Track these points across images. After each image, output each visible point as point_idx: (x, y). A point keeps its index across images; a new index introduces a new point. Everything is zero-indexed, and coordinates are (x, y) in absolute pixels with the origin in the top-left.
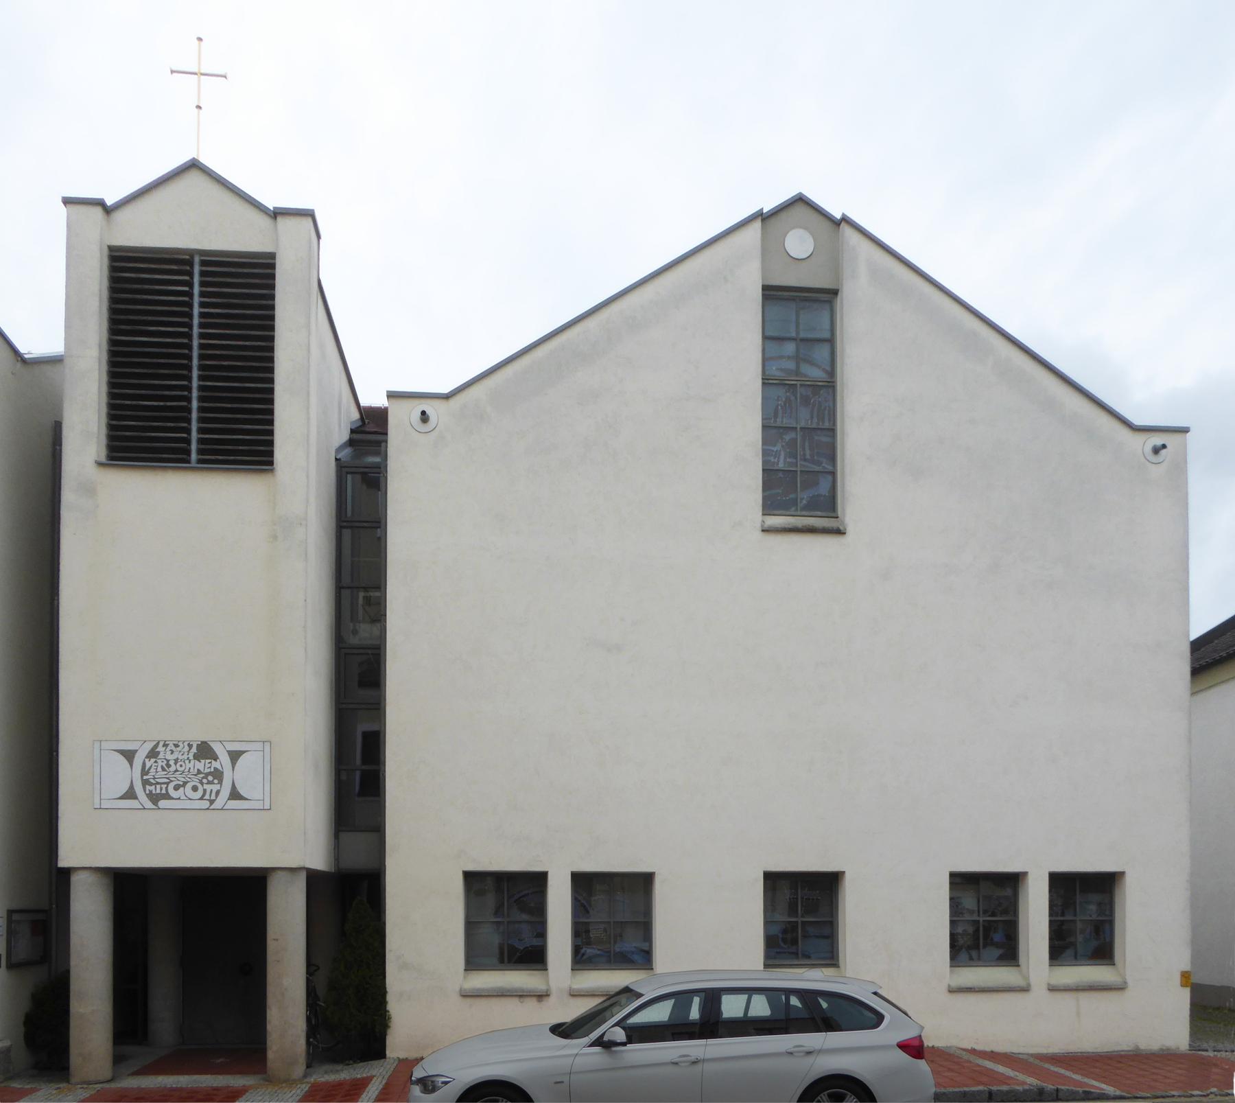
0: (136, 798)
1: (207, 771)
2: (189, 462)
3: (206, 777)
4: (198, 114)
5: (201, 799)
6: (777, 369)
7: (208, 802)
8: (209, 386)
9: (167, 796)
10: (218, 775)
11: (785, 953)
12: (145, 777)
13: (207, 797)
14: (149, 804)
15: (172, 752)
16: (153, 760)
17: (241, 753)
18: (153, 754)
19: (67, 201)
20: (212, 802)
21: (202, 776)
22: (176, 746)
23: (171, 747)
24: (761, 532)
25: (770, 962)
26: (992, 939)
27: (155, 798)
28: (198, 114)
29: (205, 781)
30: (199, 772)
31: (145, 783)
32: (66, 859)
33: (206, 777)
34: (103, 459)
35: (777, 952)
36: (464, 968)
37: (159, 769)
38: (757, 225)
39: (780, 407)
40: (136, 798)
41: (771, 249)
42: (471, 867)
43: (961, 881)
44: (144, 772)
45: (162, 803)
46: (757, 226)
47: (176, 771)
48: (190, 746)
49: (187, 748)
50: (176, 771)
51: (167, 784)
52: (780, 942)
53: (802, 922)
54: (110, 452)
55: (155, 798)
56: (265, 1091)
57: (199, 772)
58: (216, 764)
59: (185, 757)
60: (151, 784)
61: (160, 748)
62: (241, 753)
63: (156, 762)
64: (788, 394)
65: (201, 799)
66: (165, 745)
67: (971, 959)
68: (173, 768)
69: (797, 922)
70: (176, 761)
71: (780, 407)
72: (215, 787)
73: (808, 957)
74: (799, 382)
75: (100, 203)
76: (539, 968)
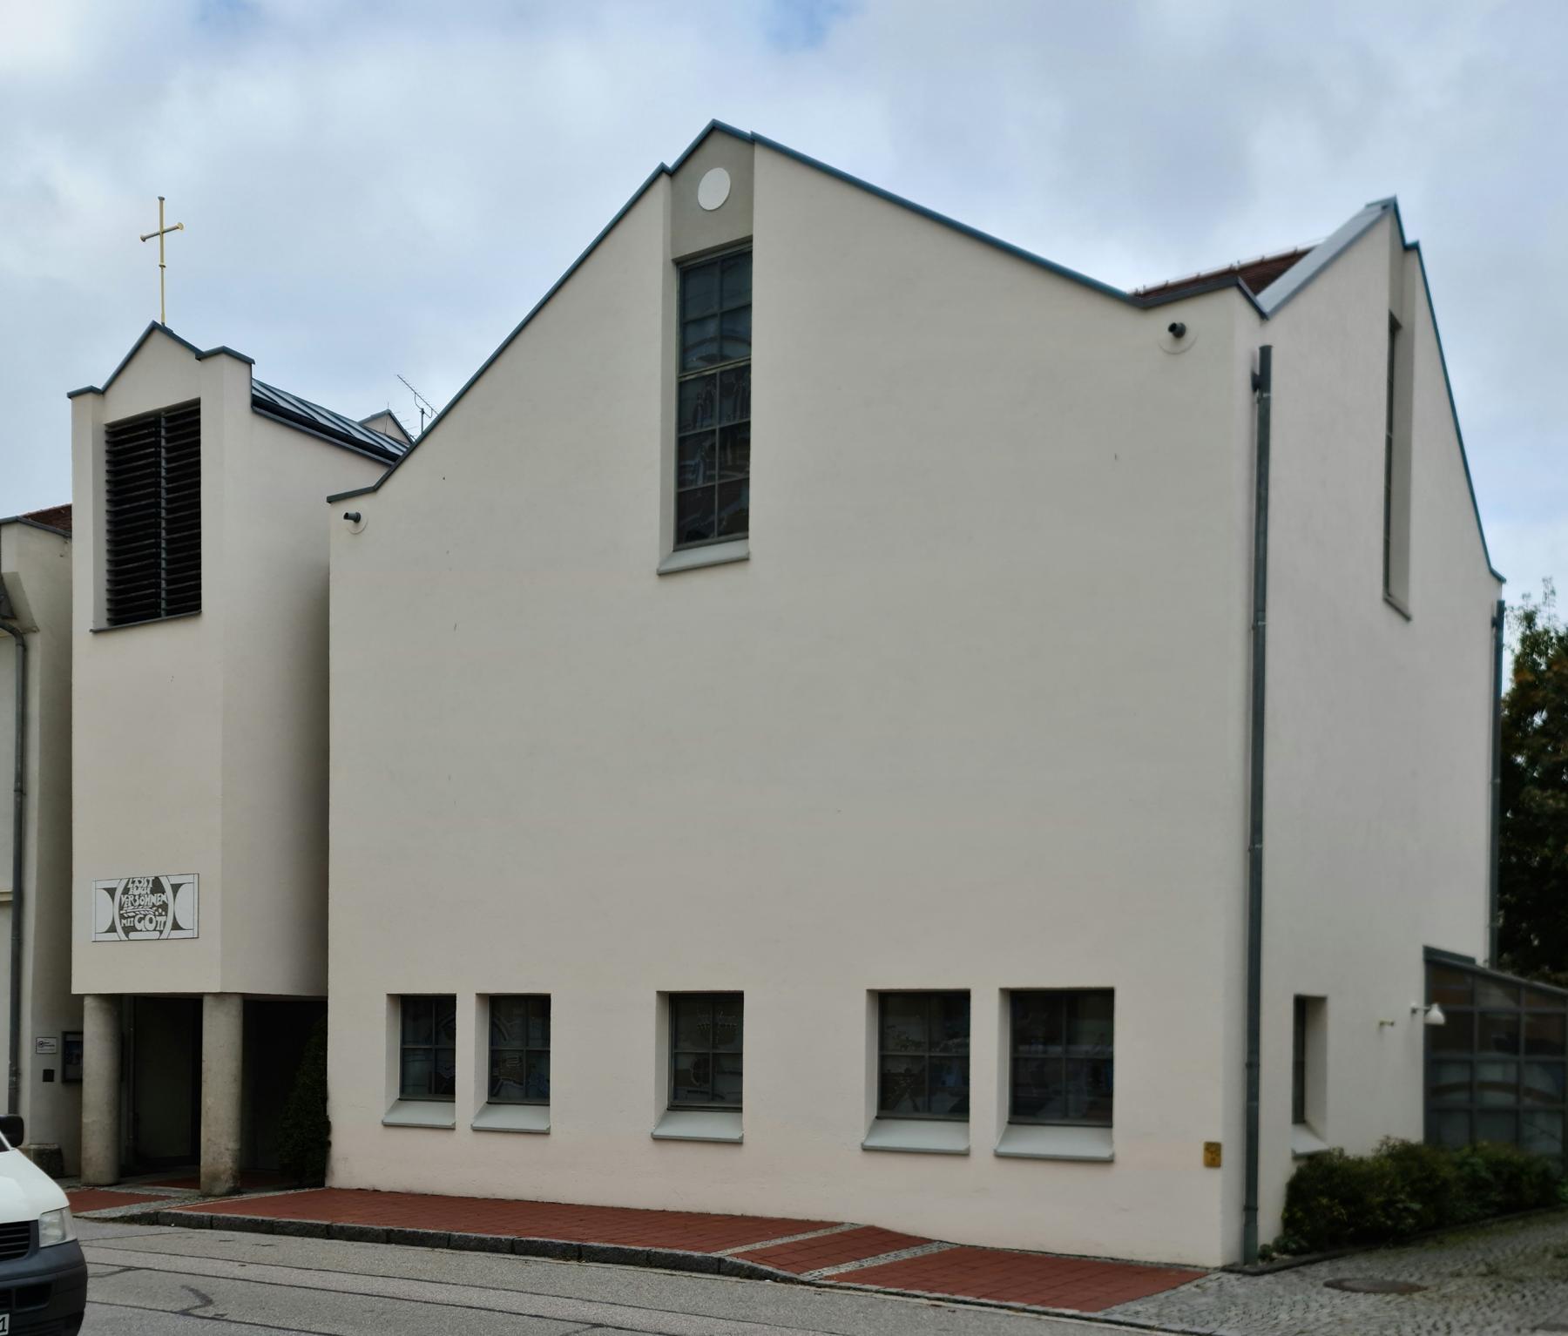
0: (115, 931)
1: (158, 904)
2: (160, 616)
3: (157, 910)
4: (162, 271)
5: (155, 930)
6: (697, 359)
7: (158, 933)
8: (175, 533)
9: (134, 929)
10: (164, 906)
11: (696, 1092)
12: (122, 912)
13: (158, 928)
14: (123, 937)
15: (137, 888)
16: (126, 896)
17: (180, 885)
18: (126, 891)
19: (71, 396)
20: (161, 932)
21: (155, 908)
22: (140, 882)
23: (137, 884)
24: (657, 577)
25: (494, 1100)
26: (944, 1083)
27: (128, 930)
28: (162, 271)
29: (157, 913)
30: (154, 905)
31: (122, 917)
32: (77, 988)
33: (157, 910)
34: (104, 624)
35: (689, 1092)
36: (1007, 1119)
37: (130, 905)
38: (664, 179)
39: (699, 408)
40: (115, 931)
41: (683, 211)
42: (478, 992)
43: (889, 1005)
44: (121, 908)
45: (133, 935)
46: (664, 179)
47: (140, 905)
48: (148, 881)
49: (146, 884)
50: (140, 905)
51: (134, 917)
52: (693, 1079)
53: (713, 1054)
54: (159, 615)
55: (128, 930)
56: (1349, 1280)
57: (154, 905)
58: (164, 897)
59: (145, 892)
60: (125, 918)
61: (130, 886)
62: (180, 885)
63: (127, 898)
64: (709, 388)
65: (155, 930)
66: (133, 882)
67: (916, 1109)
68: (137, 904)
69: (708, 1054)
70: (140, 896)
71: (699, 408)
72: (162, 919)
73: (722, 1098)
74: (719, 370)
75: (92, 390)
76: (1030, 1121)
